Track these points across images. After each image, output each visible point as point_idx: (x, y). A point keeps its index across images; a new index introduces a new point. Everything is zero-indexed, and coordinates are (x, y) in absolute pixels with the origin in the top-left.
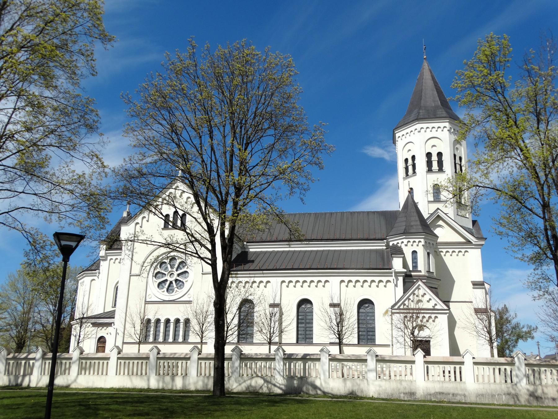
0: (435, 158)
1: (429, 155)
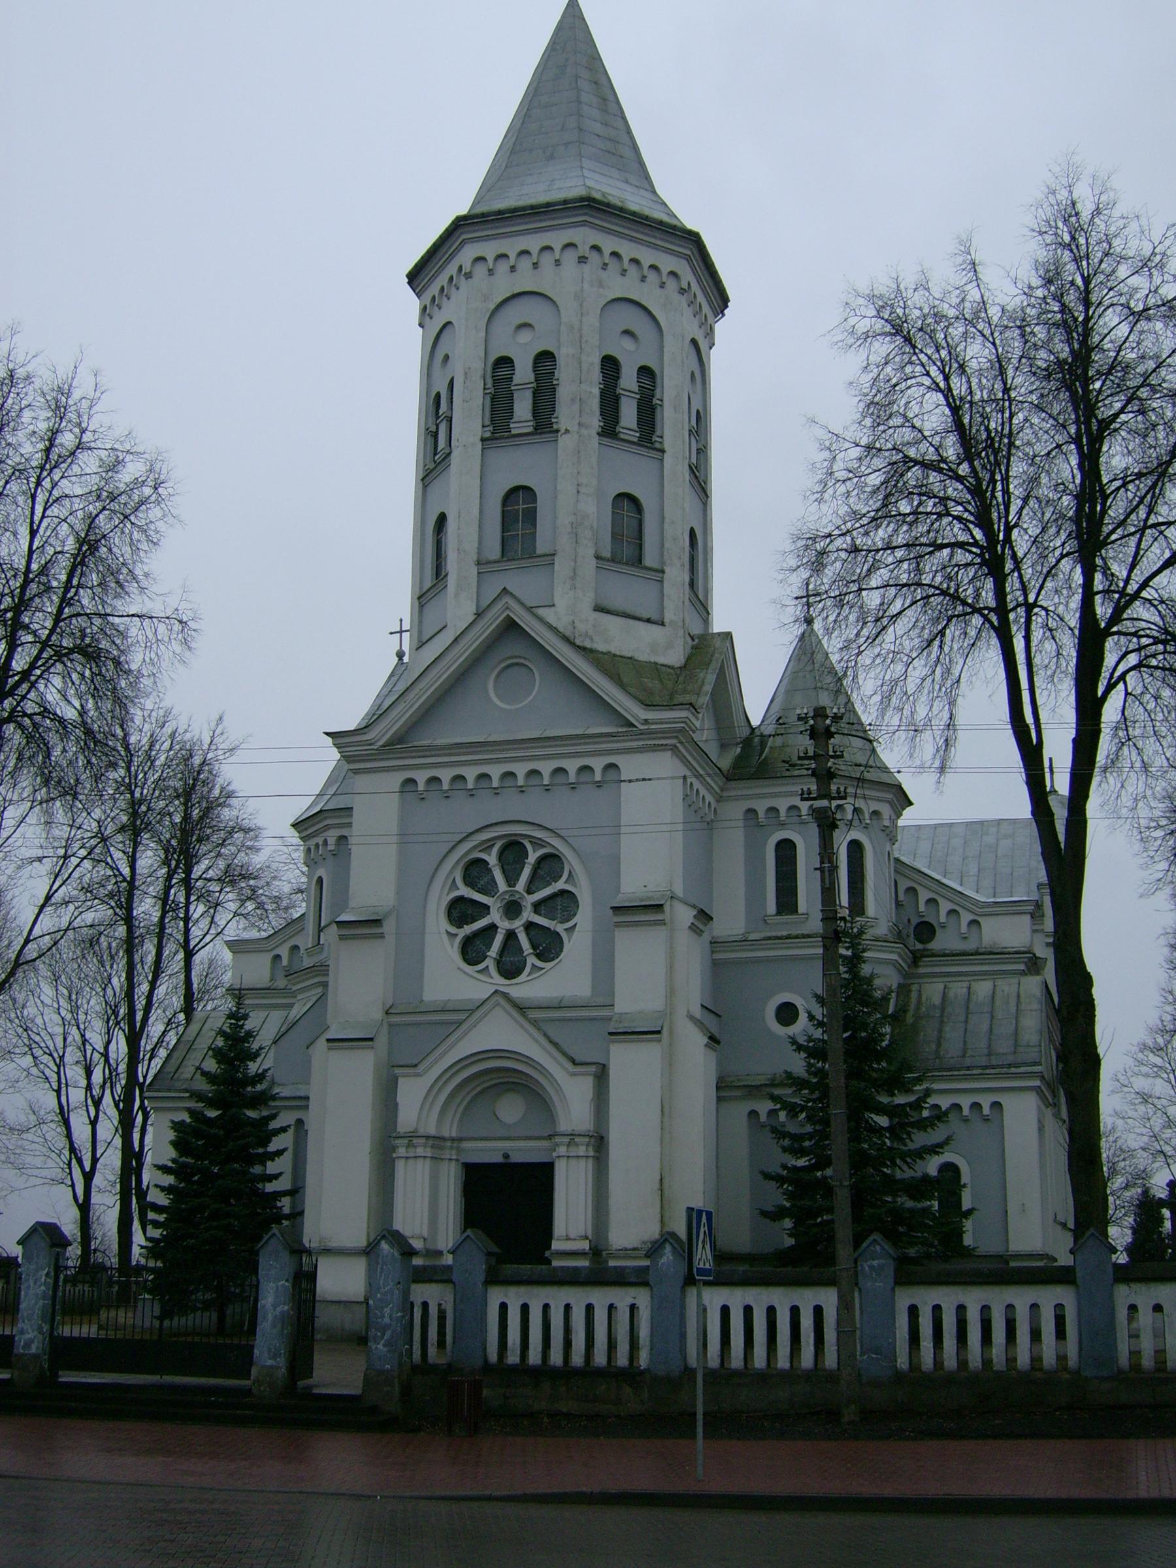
0: (628, 380)
1: (610, 365)
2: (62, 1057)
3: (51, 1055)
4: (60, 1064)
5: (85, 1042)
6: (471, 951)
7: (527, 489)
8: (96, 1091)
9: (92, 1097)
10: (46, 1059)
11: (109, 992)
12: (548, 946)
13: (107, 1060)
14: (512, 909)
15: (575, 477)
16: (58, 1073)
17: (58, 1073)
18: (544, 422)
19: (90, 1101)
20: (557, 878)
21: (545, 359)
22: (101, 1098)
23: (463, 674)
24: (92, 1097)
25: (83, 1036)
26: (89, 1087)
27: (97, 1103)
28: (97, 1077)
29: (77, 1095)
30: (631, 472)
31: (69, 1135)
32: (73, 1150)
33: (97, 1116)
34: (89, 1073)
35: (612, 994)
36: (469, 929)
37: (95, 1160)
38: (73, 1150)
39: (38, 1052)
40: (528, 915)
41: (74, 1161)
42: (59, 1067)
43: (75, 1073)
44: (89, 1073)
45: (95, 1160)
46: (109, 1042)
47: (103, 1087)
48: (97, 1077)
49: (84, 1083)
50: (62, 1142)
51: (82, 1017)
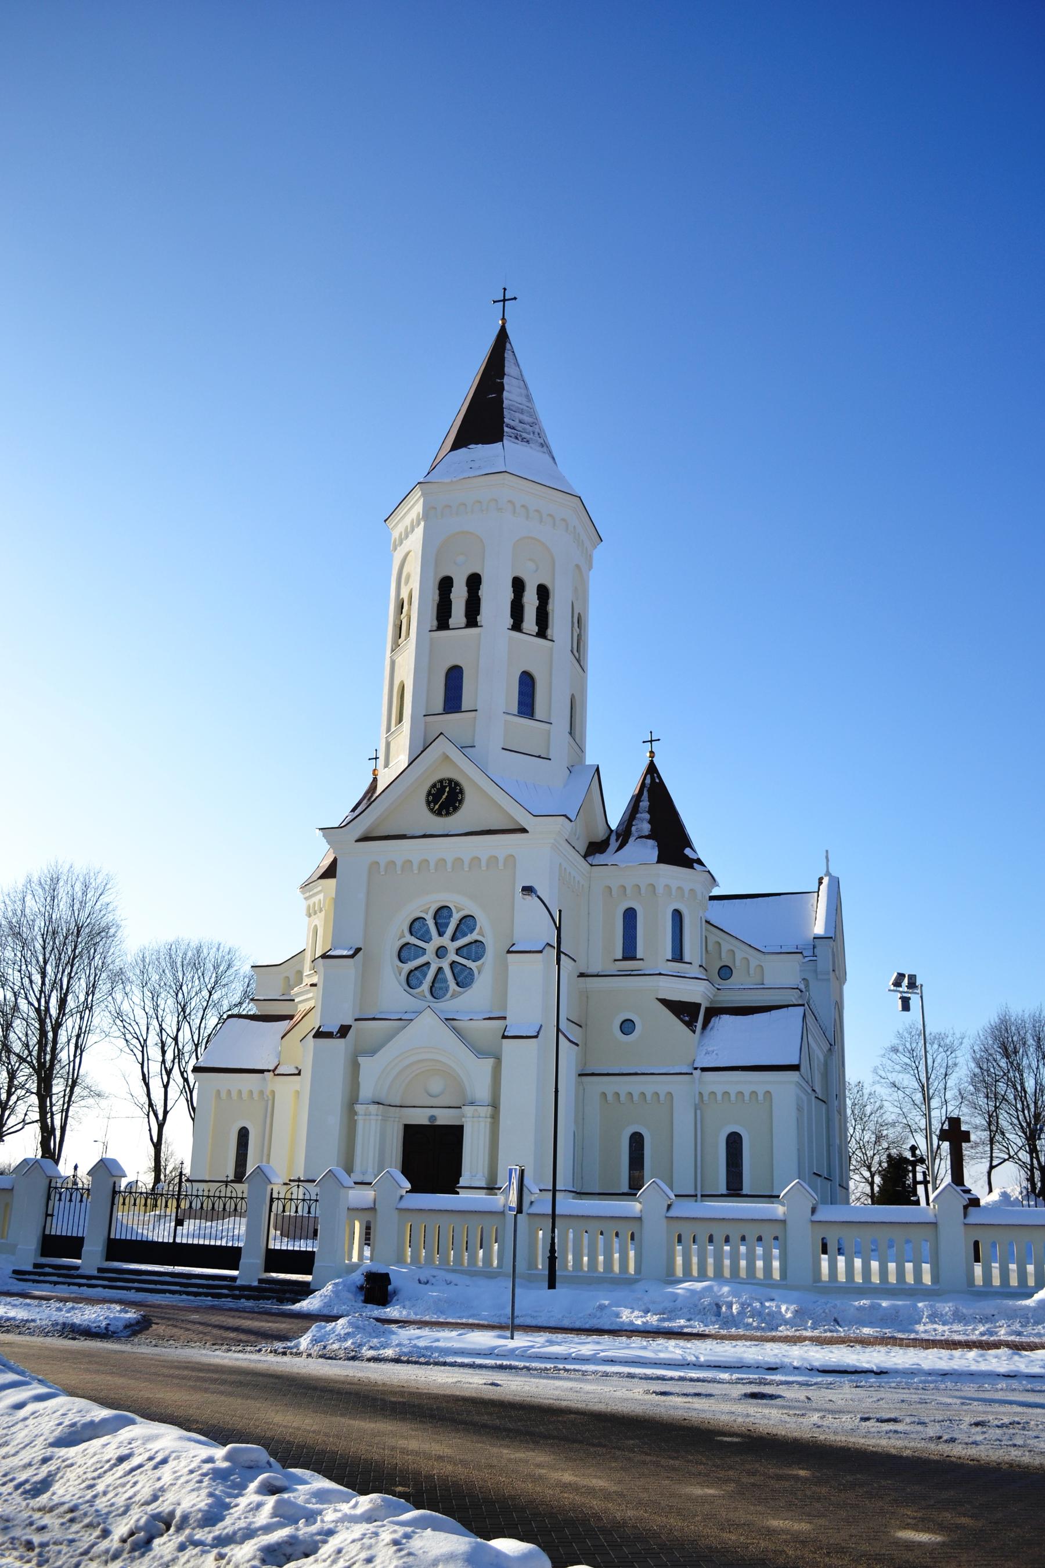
2: (145, 1041)
3: (138, 1039)
4: (144, 1045)
5: (162, 1029)
6: (411, 980)
7: (460, 859)
8: (169, 1065)
9: (166, 1068)
10: (135, 1042)
11: (180, 995)
12: (464, 978)
13: (177, 1043)
14: (441, 952)
15: (494, 651)
16: (142, 1052)
17: (142, 1052)
18: (472, 618)
19: (164, 1072)
20: (472, 931)
21: (474, 582)
22: (171, 1070)
23: (432, 1417)
24: (166, 1068)
25: (160, 1025)
26: (163, 1062)
27: (169, 1073)
28: (169, 1056)
29: (155, 1067)
30: (529, 651)
31: (149, 1095)
32: (151, 1105)
33: (168, 1082)
34: (164, 1052)
35: (504, 1007)
36: (413, 940)
37: (166, 1113)
38: (151, 1105)
39: (129, 1037)
40: (452, 956)
41: (151, 1113)
42: (143, 1047)
43: (154, 1052)
44: (164, 1052)
45: (166, 1113)
46: (178, 1030)
47: (173, 1061)
48: (169, 1056)
49: (161, 1059)
50: (145, 1100)
51: (160, 1012)
